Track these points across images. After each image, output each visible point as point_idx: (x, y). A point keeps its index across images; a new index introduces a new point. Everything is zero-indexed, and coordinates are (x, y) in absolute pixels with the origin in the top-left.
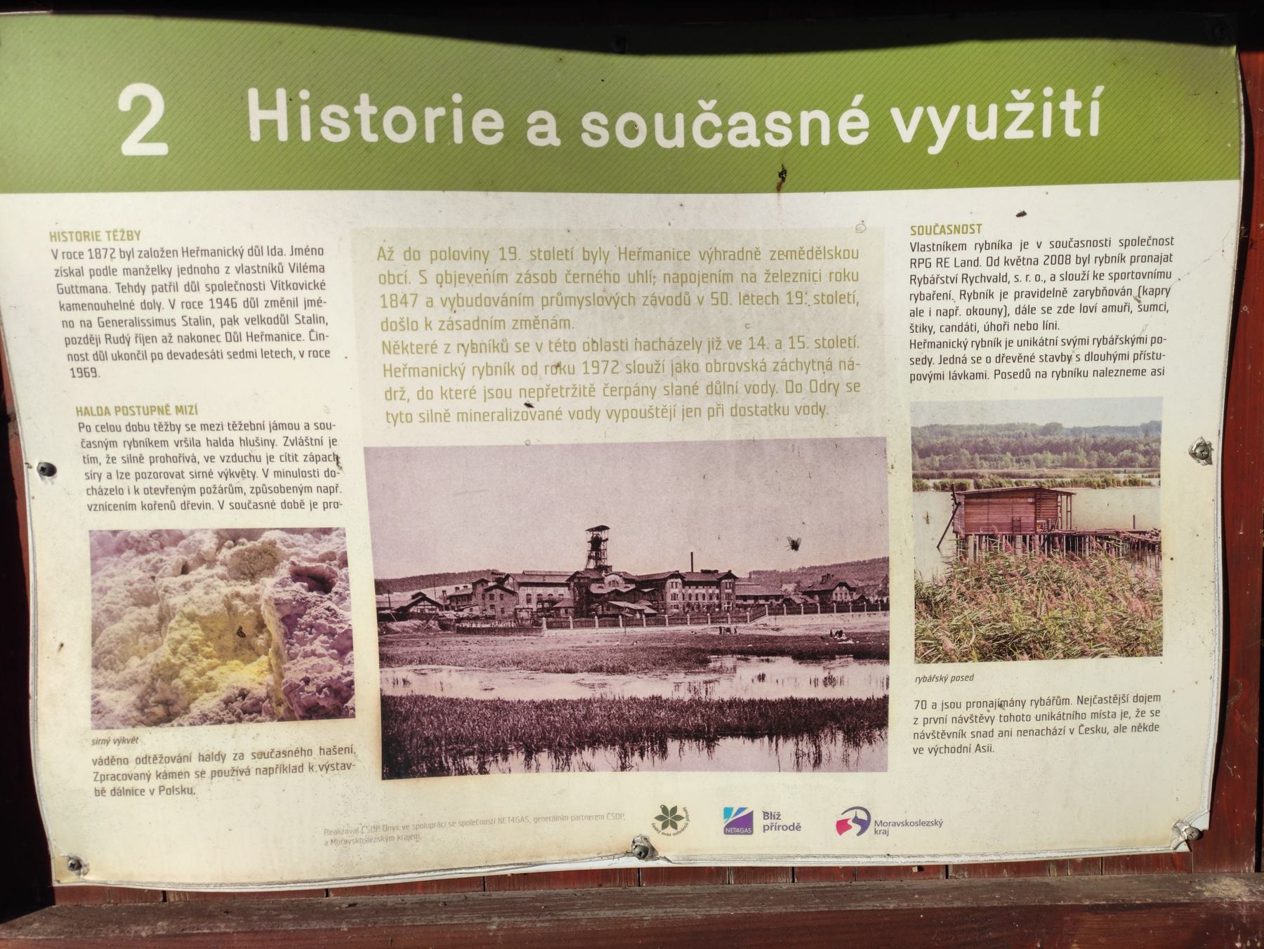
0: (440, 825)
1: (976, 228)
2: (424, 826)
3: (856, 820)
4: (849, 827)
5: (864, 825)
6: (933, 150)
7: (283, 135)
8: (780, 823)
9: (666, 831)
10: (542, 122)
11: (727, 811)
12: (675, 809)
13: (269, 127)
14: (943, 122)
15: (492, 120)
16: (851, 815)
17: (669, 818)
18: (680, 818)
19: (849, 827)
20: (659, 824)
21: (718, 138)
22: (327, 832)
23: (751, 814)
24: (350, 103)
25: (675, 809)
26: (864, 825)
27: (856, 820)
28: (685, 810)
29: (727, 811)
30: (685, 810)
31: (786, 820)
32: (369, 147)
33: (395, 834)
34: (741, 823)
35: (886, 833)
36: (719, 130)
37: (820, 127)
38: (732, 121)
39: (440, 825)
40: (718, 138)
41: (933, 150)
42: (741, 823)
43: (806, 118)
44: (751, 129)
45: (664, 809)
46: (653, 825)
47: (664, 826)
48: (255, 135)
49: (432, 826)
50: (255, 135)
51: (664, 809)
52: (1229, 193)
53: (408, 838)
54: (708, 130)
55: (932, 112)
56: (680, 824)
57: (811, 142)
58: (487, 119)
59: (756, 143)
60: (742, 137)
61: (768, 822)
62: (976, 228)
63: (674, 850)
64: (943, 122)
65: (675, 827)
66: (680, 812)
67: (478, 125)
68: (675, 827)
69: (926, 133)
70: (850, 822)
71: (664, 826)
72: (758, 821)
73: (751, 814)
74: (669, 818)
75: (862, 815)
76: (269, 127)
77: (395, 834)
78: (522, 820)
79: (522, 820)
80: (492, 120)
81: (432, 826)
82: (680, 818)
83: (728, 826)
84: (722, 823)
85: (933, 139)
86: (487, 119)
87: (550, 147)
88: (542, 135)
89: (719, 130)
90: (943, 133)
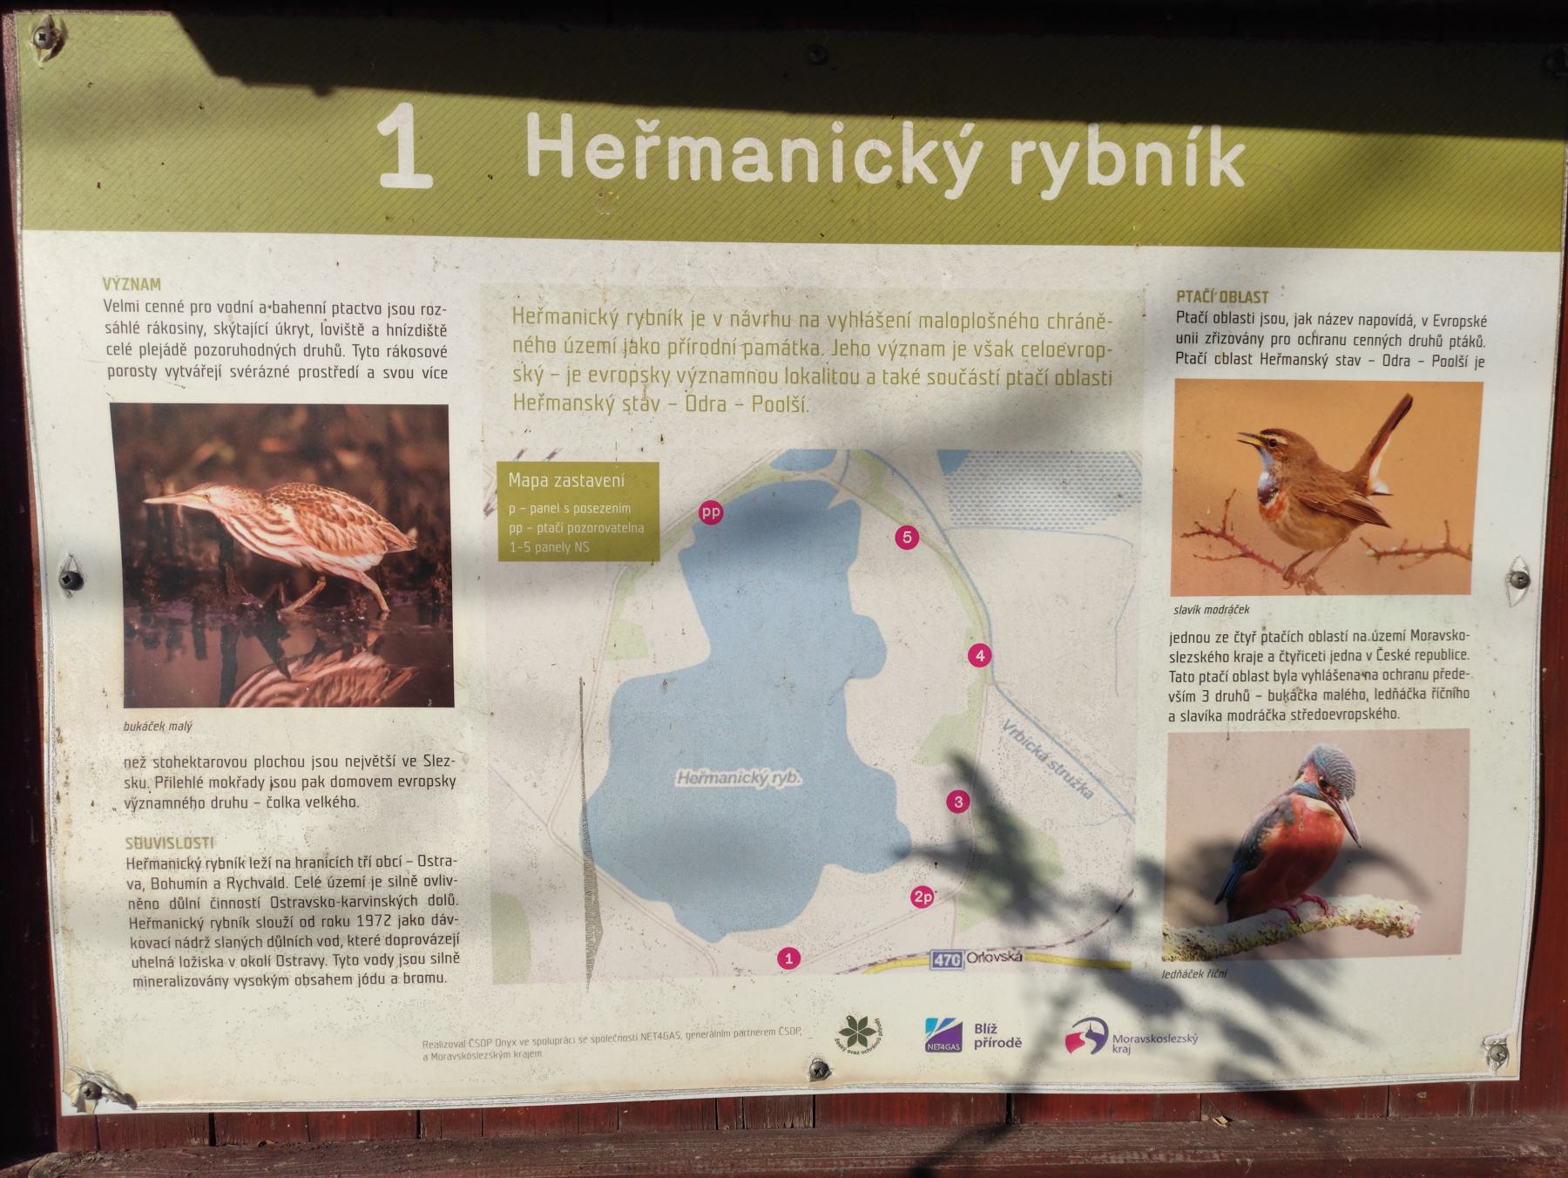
0: (568, 1041)
1: (1261, 296)
2: (547, 1041)
3: (1090, 1034)
4: (1082, 1043)
5: (1100, 1040)
6: (1049, 195)
7: (567, 170)
8: (995, 1037)
9: (852, 1048)
10: (751, 151)
11: (931, 1023)
12: (865, 1021)
13: (550, 160)
14: (1059, 161)
15: (611, 149)
16: (1083, 1029)
17: (857, 1032)
18: (871, 1032)
19: (1082, 1043)
20: (844, 1040)
21: (886, 172)
22: (426, 1044)
23: (960, 1026)
24: (639, 132)
25: (865, 1021)
26: (1100, 1040)
27: (1090, 1034)
28: (877, 1021)
29: (931, 1023)
30: (877, 1021)
31: (1002, 1035)
32: (603, 187)
33: (512, 1049)
34: (947, 1038)
35: (1127, 1050)
36: (888, 161)
37: (1160, 164)
38: (739, 147)
39: (568, 1041)
40: (886, 172)
41: (1049, 195)
42: (947, 1038)
43: (788, 147)
44: (762, 157)
45: (851, 1020)
46: (837, 1041)
47: (851, 1043)
48: (534, 169)
49: (556, 1042)
50: (534, 169)
51: (851, 1020)
52: (1555, 260)
53: (528, 1055)
54: (874, 162)
55: (1046, 149)
56: (871, 1039)
57: (575, 173)
58: (604, 147)
59: (768, 177)
60: (750, 168)
61: (981, 1037)
62: (1261, 296)
63: (859, 1073)
64: (1059, 161)
65: (864, 1042)
66: (871, 1025)
67: (592, 156)
68: (864, 1042)
69: (1036, 169)
70: (1083, 1037)
71: (851, 1043)
72: (968, 1036)
73: (960, 1026)
74: (857, 1032)
75: (1098, 1029)
76: (550, 160)
77: (512, 1049)
78: (672, 1035)
79: (672, 1035)
80: (611, 149)
81: (556, 1042)
82: (871, 1032)
83: (931, 1041)
84: (923, 1037)
85: (1047, 182)
86: (604, 147)
87: (760, 182)
88: (750, 168)
89: (888, 161)
90: (1059, 174)
